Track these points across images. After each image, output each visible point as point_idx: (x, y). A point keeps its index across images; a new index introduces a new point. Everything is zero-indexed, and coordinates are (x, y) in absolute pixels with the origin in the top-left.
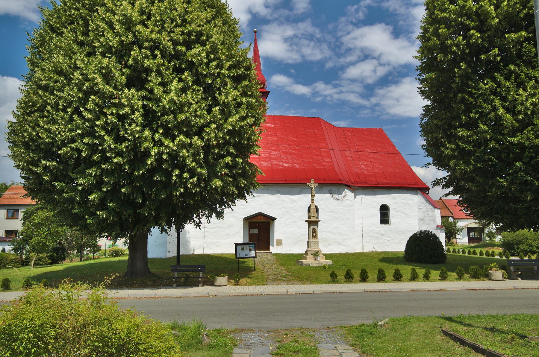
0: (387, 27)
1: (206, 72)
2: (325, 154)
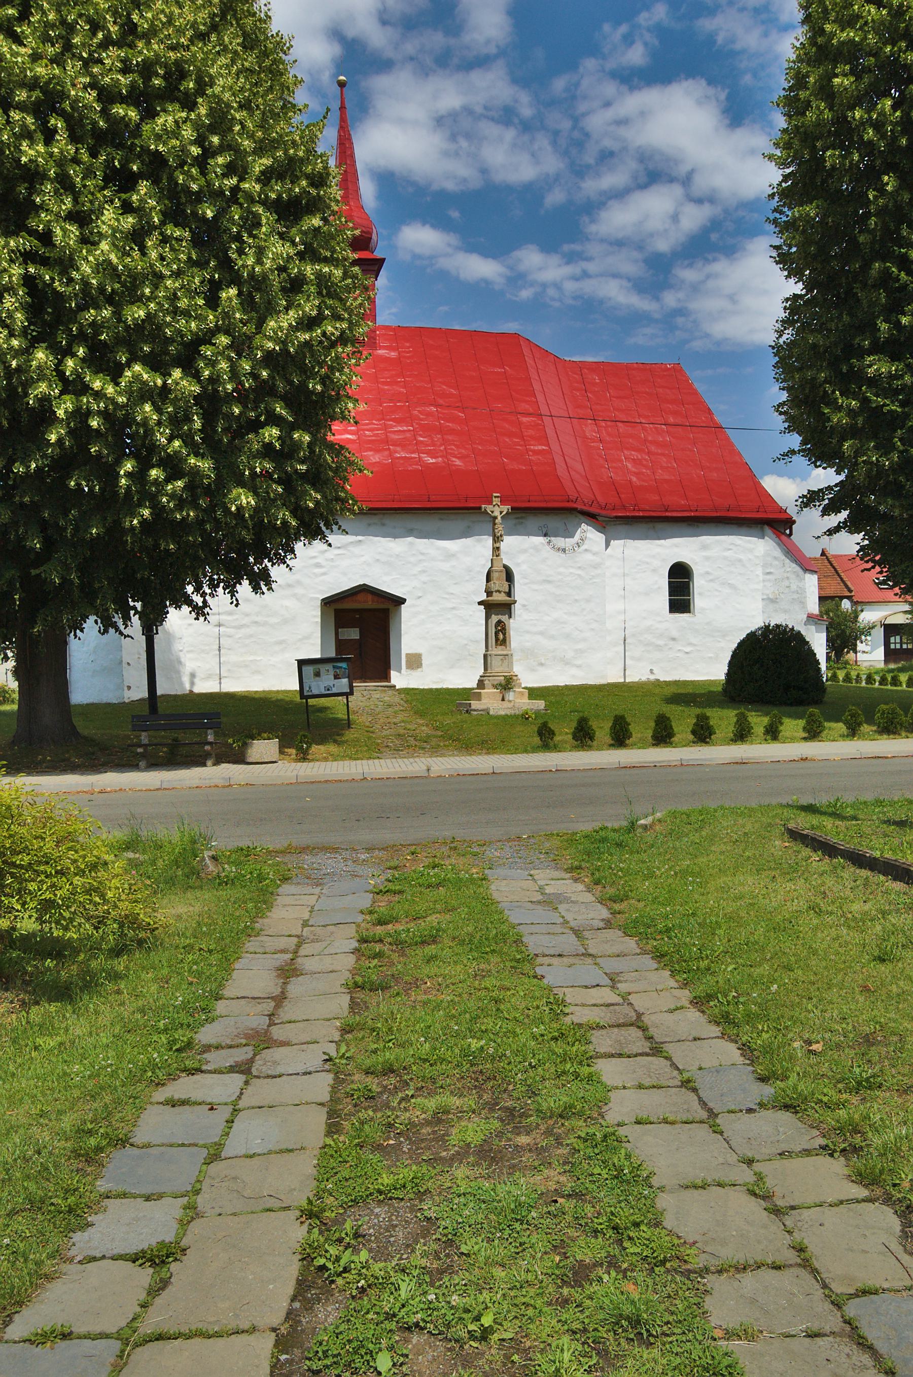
0: (711, 91)
1: (200, 187)
2: (531, 432)
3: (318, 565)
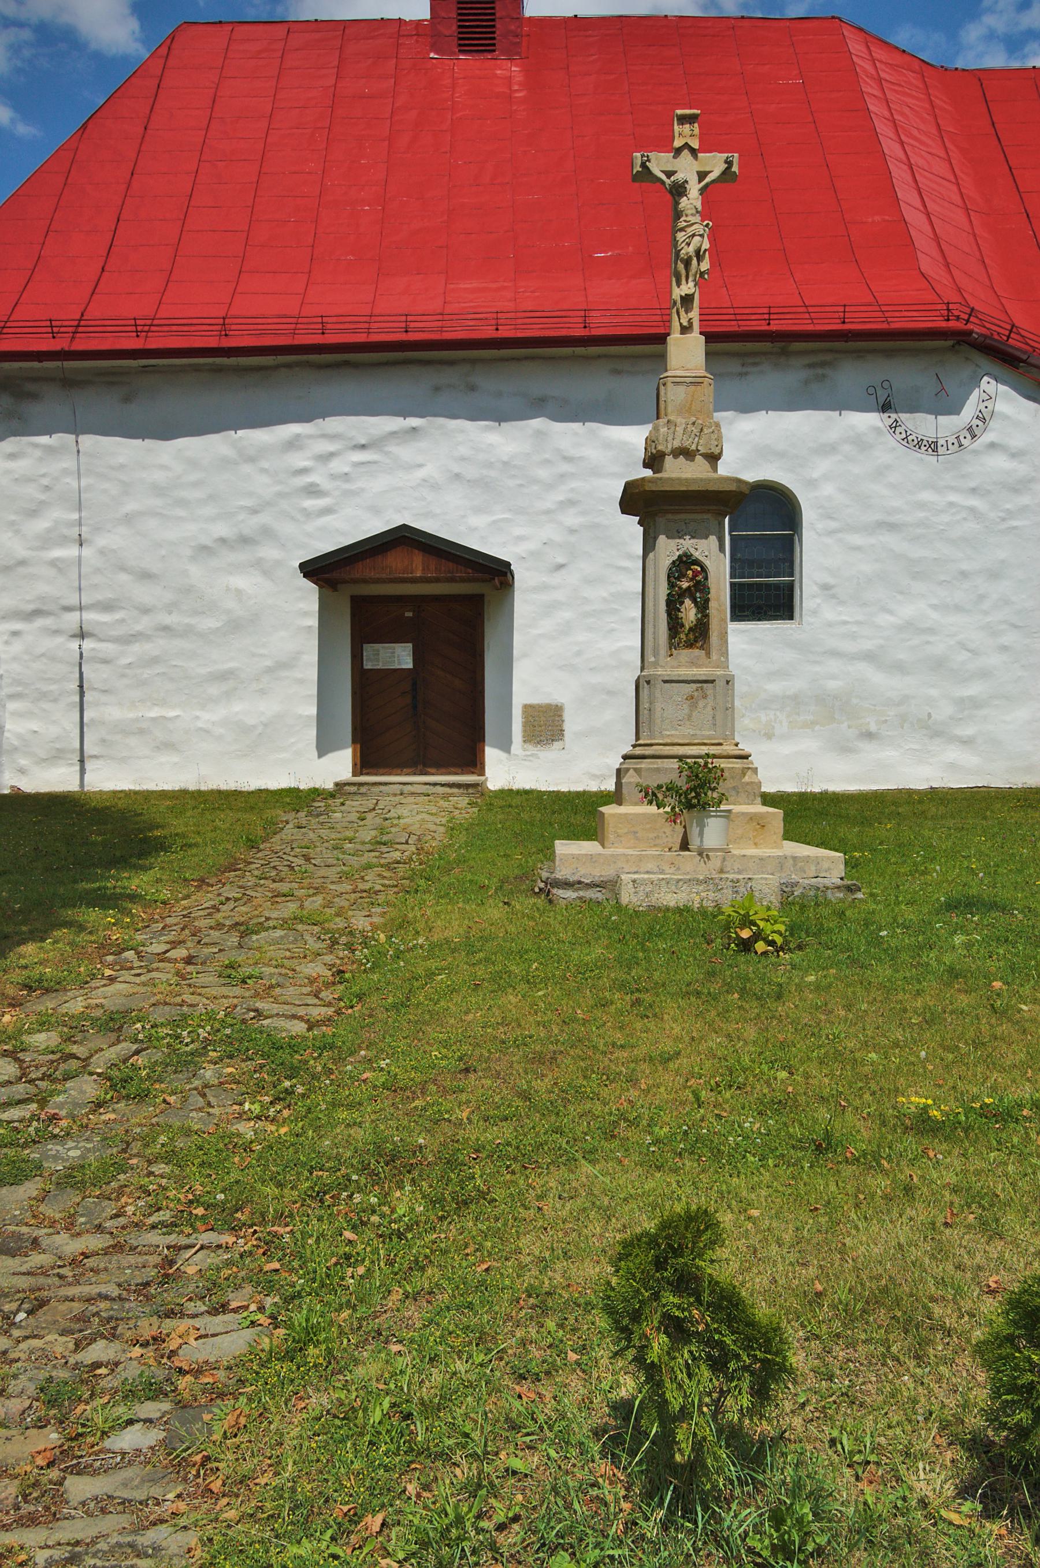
3: (313, 491)
